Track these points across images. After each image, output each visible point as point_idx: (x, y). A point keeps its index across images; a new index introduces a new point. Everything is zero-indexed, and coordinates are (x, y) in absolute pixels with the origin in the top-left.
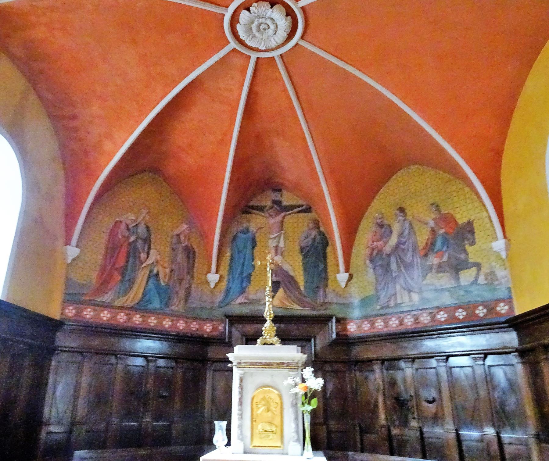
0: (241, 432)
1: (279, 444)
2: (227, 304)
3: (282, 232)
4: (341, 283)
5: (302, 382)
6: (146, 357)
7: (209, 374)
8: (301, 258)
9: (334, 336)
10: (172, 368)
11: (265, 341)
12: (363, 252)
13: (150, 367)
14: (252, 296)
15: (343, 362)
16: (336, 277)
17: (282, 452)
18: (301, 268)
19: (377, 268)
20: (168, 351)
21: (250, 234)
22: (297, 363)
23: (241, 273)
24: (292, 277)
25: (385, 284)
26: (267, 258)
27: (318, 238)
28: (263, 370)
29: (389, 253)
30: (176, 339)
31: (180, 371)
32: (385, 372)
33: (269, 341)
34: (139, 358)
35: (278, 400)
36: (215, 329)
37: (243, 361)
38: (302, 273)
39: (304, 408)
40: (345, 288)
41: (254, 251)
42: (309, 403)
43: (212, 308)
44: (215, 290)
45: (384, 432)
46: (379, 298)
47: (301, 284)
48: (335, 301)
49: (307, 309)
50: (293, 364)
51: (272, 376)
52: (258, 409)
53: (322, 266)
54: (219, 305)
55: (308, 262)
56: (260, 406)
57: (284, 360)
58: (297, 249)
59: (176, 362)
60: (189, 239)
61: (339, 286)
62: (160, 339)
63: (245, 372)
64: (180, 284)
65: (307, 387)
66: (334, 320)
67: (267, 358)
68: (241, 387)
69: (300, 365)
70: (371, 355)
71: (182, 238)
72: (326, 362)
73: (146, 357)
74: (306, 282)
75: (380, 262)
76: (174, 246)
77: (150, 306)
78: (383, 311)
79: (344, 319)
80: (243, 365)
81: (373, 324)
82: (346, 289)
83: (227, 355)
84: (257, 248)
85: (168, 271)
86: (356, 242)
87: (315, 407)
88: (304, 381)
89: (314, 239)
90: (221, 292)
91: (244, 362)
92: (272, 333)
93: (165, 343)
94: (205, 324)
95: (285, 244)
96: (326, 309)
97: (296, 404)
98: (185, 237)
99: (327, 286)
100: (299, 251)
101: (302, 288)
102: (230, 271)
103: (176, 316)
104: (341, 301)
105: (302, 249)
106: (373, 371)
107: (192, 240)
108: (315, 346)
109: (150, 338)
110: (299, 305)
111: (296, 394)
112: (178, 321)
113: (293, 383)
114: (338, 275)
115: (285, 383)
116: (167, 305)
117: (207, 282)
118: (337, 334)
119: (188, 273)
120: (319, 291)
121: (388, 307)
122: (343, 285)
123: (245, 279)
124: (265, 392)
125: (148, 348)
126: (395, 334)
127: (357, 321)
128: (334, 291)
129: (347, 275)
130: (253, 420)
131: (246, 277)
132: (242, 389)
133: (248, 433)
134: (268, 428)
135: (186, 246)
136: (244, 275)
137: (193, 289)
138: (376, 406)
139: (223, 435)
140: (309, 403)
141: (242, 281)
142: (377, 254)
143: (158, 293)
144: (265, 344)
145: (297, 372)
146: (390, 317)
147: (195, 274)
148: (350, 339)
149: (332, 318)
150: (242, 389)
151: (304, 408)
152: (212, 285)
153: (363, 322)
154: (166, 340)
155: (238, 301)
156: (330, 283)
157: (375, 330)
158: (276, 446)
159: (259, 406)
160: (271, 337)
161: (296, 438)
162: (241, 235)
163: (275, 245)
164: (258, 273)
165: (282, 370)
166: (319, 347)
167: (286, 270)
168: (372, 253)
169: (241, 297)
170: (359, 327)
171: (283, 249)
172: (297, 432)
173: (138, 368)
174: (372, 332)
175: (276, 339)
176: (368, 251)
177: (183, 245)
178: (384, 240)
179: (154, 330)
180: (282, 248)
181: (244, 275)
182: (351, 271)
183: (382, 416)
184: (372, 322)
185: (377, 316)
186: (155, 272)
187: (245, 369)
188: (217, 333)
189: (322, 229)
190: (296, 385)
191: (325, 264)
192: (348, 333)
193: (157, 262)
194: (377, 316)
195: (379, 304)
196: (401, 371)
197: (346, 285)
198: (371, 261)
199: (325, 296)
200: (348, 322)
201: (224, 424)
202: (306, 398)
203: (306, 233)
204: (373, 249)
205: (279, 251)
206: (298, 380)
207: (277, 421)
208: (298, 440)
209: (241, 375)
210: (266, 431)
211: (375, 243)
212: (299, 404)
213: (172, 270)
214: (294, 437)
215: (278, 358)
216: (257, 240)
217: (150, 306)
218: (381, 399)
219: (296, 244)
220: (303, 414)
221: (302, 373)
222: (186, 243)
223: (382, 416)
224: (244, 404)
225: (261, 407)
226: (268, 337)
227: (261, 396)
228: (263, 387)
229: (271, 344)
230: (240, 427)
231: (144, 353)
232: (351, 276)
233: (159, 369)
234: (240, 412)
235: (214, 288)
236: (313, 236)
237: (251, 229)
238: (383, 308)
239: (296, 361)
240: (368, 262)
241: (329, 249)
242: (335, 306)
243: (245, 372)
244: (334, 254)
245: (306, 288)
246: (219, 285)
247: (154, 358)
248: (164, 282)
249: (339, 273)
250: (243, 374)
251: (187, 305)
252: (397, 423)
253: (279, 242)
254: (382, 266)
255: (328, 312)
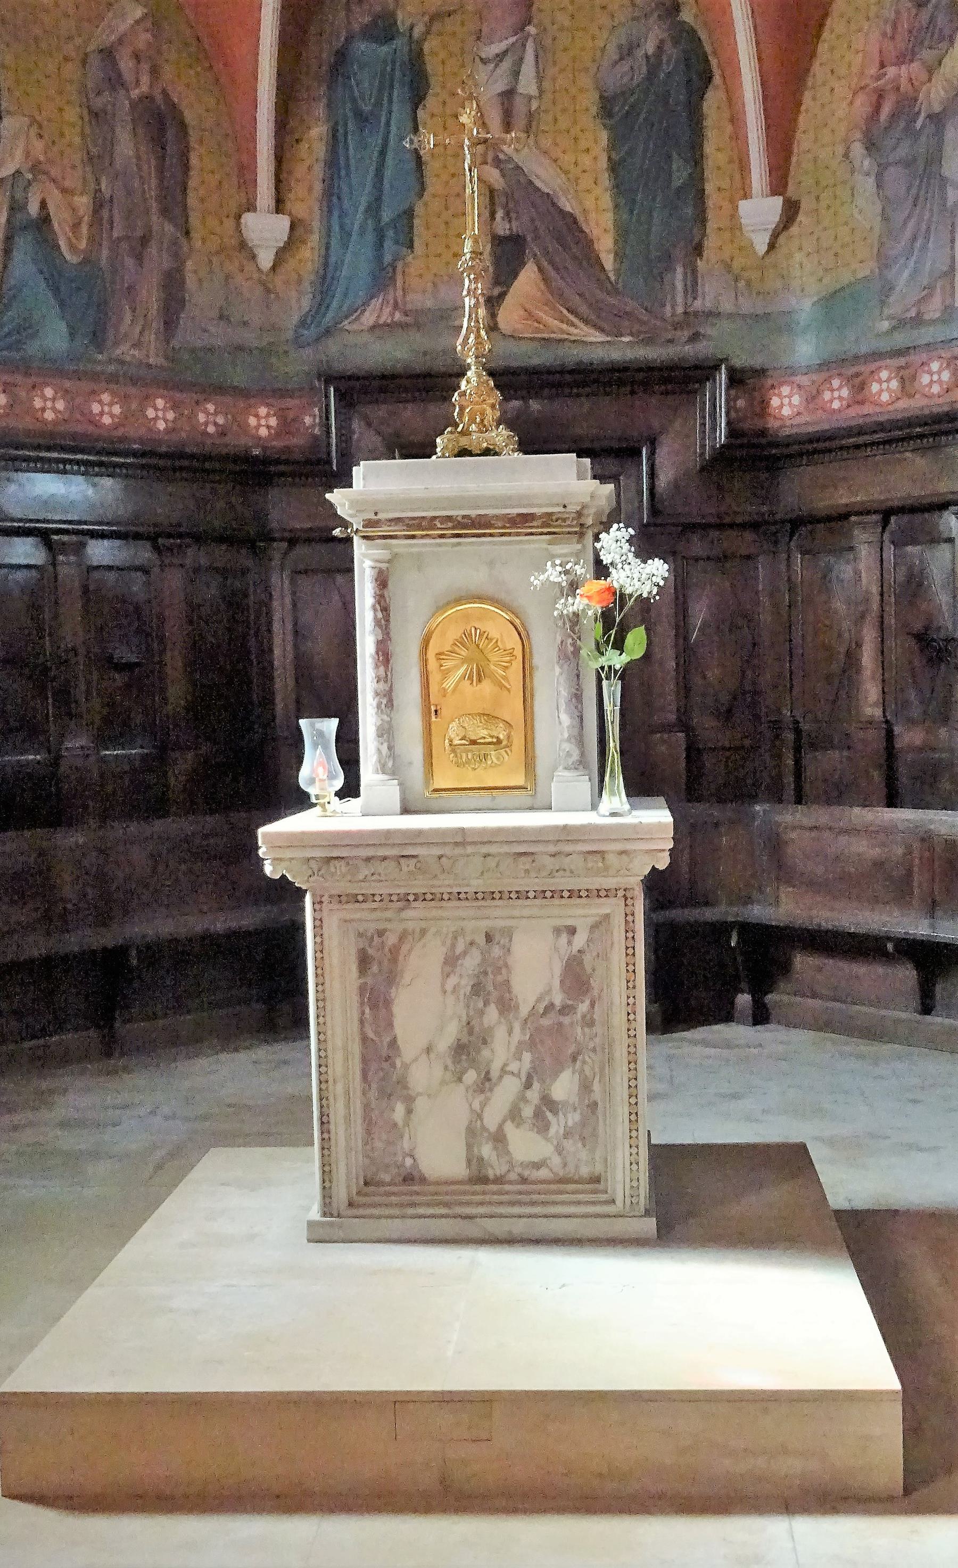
0: (390, 748)
1: (520, 780)
2: (328, 332)
3: (531, 29)
4: (753, 236)
5: (598, 578)
6: (44, 536)
7: (280, 582)
8: (604, 136)
9: (722, 436)
10: (145, 570)
11: (464, 442)
12: (841, 110)
13: (63, 571)
14: (416, 300)
15: (754, 526)
16: (734, 214)
17: (529, 802)
18: (605, 180)
19: (893, 173)
20: (124, 511)
21: (398, 43)
22: (579, 514)
23: (374, 208)
24: (571, 222)
25: (914, 238)
26: (464, 119)
27: (672, 52)
28: (459, 544)
29: (937, 108)
30: (143, 467)
31: (174, 581)
32: (890, 552)
33: (477, 440)
34: (17, 540)
35: (513, 641)
36: (287, 425)
37: (382, 516)
38: (607, 200)
39: (603, 661)
40: (768, 252)
41: (421, 113)
42: (619, 645)
43: (267, 351)
44: (278, 281)
45: (875, 738)
46: (888, 289)
47: (605, 246)
48: (727, 306)
49: (626, 339)
50: (564, 520)
51: (491, 564)
52: (446, 674)
53: (680, 173)
54: (297, 337)
55: (631, 152)
56: (453, 663)
57: (531, 506)
58: (590, 101)
59: (157, 549)
60: (155, 71)
61: (748, 248)
62: (89, 469)
63: (395, 556)
64: (139, 258)
65: (610, 590)
66: (723, 377)
67: (475, 502)
68: (383, 606)
69: (589, 521)
70: (843, 498)
71: (126, 64)
72: (691, 527)
73: (44, 536)
74: (622, 233)
75: (903, 151)
76: (98, 103)
77: (33, 348)
78: (900, 339)
79: (761, 373)
80: (384, 530)
81: (859, 387)
82: (772, 257)
83: (328, 496)
84: (431, 102)
85: (83, 202)
86: (818, 70)
87: (639, 653)
88: (601, 570)
89: (654, 62)
90: (300, 281)
91: (391, 520)
92: (489, 411)
93: (107, 482)
94: (247, 410)
95: (540, 78)
96: (695, 337)
97: (577, 651)
98: (137, 57)
99: (698, 250)
100: (594, 110)
101: (608, 262)
102: (331, 195)
103: (134, 381)
104: (746, 305)
105: (607, 106)
106: (851, 549)
107: (168, 72)
108: (652, 475)
109: (47, 466)
110: (595, 326)
111: (575, 619)
112: (147, 399)
113: (563, 580)
114: (744, 205)
115: (537, 580)
116: (98, 338)
117: (244, 248)
118: (733, 432)
119: (165, 212)
120: (670, 269)
121: (918, 321)
122: (761, 243)
123: (390, 233)
124: (466, 616)
125: (46, 503)
126: (937, 419)
127: (804, 380)
128: (728, 267)
129: (777, 202)
130: (430, 711)
131: (394, 223)
132: (385, 610)
133: (414, 752)
134: (482, 733)
135: (149, 98)
136: (387, 216)
137: (191, 282)
138: (852, 659)
139: (329, 759)
140: (619, 645)
141: (379, 244)
142: (894, 116)
143: (56, 291)
144: (464, 452)
145: (579, 546)
146: (924, 356)
147: (194, 220)
148: (776, 445)
149: (717, 367)
150: (385, 610)
151: (603, 661)
152: (266, 259)
153: (828, 380)
154: (109, 470)
155: (369, 318)
156: (711, 242)
157: (867, 409)
158: (512, 784)
159: (448, 664)
160: (483, 428)
161: (576, 756)
162: (362, 47)
163: (501, 86)
164: (436, 205)
165: (528, 542)
166: (664, 479)
167: (546, 190)
168: (877, 108)
169: (376, 303)
170: (812, 398)
171: (534, 105)
172: (580, 740)
173: (20, 575)
174: (855, 415)
175: (501, 436)
176: (862, 105)
177: (135, 93)
178: (927, 55)
179: (52, 435)
180: (530, 98)
181: (387, 216)
182: (791, 191)
183: (870, 692)
184: (857, 381)
185: (876, 356)
186: (33, 209)
187: (394, 542)
188: (297, 441)
189: (687, 16)
190: (573, 587)
191: (696, 158)
192: (772, 424)
193: (36, 168)
194: (876, 356)
195: (886, 312)
196: (945, 546)
197: (772, 246)
198: (871, 146)
199: (692, 289)
200: (769, 382)
201: (332, 725)
202: (607, 627)
203: (621, 37)
204: (880, 96)
205: (520, 107)
206: (582, 570)
207: (513, 708)
208: (582, 763)
209: (378, 565)
210: (474, 742)
211: (891, 71)
212: (587, 649)
213: (99, 205)
214: (569, 754)
215: (505, 500)
216: (432, 65)
217: (33, 348)
218: (869, 636)
219: (586, 81)
220: (599, 680)
221: (598, 545)
222: (144, 88)
223: (870, 692)
224: (397, 662)
225: (457, 667)
226: (473, 427)
227: (454, 633)
228: (458, 601)
229: (487, 452)
230: (386, 732)
231: (31, 521)
232: (791, 211)
233: (96, 575)
234: (382, 686)
235: (274, 268)
236: (650, 47)
237: (403, 19)
238: (900, 324)
239: (573, 508)
240: (858, 149)
241: (712, 101)
242: (725, 325)
243: (395, 556)
244: (732, 120)
245: (619, 256)
246: (291, 263)
247: (74, 538)
248: (72, 247)
249: (746, 196)
250: (389, 562)
251: (175, 343)
252: (916, 711)
253: (516, 74)
254: (908, 163)
255: (702, 350)
